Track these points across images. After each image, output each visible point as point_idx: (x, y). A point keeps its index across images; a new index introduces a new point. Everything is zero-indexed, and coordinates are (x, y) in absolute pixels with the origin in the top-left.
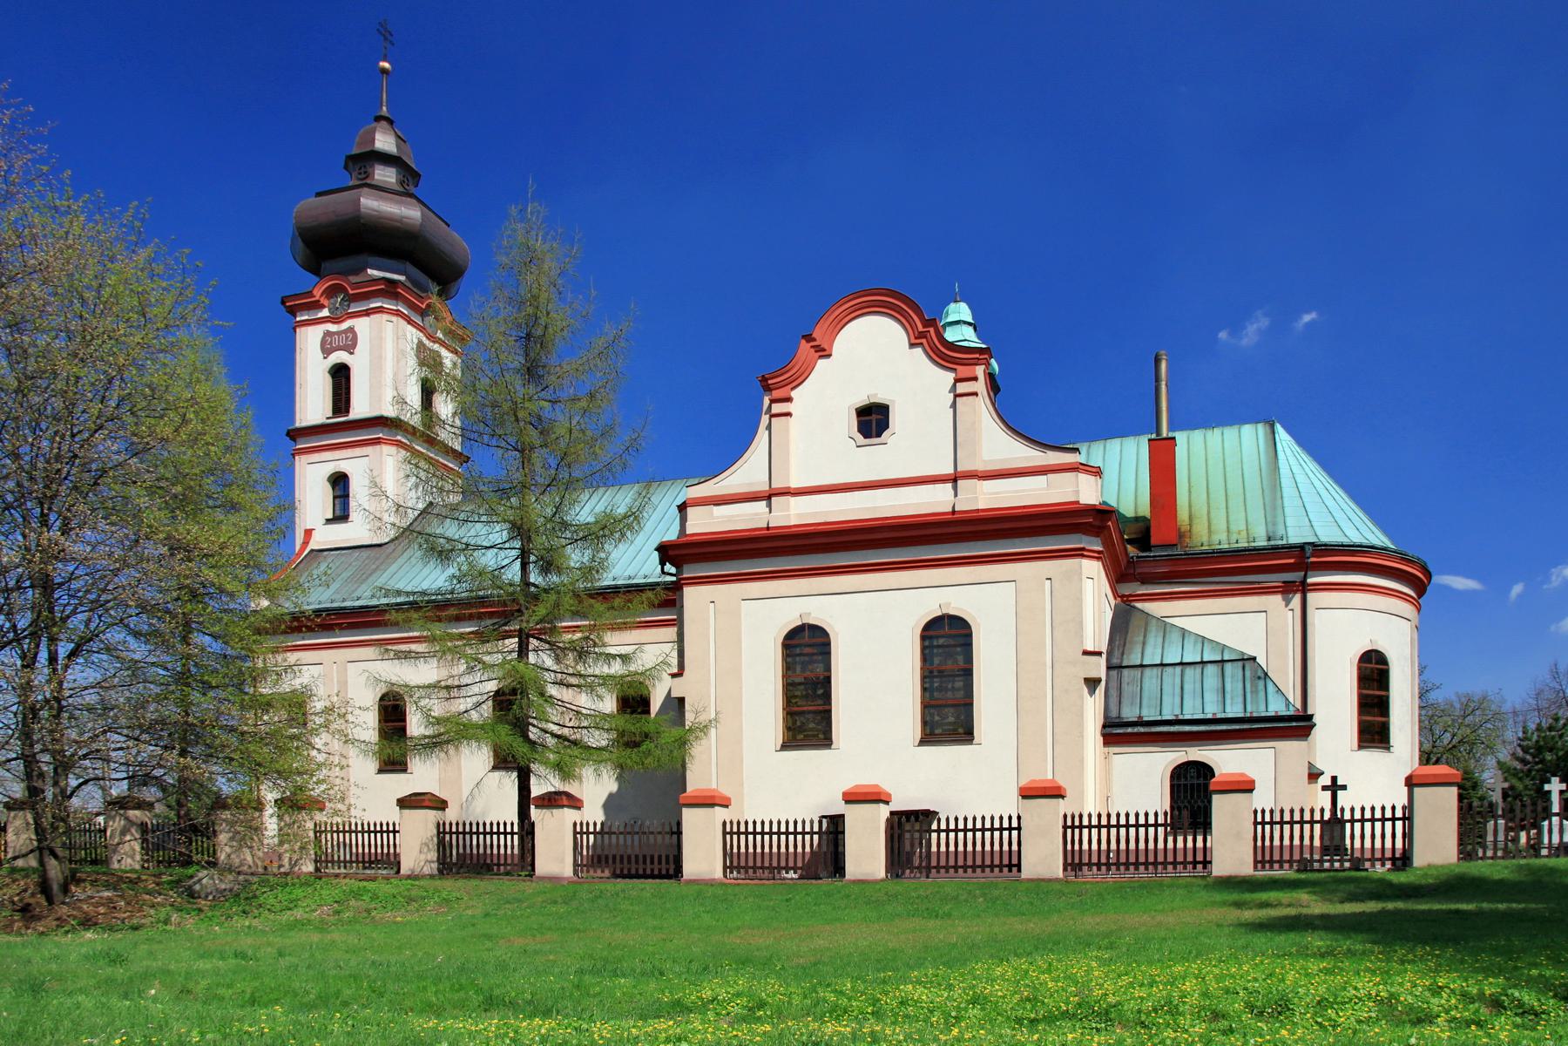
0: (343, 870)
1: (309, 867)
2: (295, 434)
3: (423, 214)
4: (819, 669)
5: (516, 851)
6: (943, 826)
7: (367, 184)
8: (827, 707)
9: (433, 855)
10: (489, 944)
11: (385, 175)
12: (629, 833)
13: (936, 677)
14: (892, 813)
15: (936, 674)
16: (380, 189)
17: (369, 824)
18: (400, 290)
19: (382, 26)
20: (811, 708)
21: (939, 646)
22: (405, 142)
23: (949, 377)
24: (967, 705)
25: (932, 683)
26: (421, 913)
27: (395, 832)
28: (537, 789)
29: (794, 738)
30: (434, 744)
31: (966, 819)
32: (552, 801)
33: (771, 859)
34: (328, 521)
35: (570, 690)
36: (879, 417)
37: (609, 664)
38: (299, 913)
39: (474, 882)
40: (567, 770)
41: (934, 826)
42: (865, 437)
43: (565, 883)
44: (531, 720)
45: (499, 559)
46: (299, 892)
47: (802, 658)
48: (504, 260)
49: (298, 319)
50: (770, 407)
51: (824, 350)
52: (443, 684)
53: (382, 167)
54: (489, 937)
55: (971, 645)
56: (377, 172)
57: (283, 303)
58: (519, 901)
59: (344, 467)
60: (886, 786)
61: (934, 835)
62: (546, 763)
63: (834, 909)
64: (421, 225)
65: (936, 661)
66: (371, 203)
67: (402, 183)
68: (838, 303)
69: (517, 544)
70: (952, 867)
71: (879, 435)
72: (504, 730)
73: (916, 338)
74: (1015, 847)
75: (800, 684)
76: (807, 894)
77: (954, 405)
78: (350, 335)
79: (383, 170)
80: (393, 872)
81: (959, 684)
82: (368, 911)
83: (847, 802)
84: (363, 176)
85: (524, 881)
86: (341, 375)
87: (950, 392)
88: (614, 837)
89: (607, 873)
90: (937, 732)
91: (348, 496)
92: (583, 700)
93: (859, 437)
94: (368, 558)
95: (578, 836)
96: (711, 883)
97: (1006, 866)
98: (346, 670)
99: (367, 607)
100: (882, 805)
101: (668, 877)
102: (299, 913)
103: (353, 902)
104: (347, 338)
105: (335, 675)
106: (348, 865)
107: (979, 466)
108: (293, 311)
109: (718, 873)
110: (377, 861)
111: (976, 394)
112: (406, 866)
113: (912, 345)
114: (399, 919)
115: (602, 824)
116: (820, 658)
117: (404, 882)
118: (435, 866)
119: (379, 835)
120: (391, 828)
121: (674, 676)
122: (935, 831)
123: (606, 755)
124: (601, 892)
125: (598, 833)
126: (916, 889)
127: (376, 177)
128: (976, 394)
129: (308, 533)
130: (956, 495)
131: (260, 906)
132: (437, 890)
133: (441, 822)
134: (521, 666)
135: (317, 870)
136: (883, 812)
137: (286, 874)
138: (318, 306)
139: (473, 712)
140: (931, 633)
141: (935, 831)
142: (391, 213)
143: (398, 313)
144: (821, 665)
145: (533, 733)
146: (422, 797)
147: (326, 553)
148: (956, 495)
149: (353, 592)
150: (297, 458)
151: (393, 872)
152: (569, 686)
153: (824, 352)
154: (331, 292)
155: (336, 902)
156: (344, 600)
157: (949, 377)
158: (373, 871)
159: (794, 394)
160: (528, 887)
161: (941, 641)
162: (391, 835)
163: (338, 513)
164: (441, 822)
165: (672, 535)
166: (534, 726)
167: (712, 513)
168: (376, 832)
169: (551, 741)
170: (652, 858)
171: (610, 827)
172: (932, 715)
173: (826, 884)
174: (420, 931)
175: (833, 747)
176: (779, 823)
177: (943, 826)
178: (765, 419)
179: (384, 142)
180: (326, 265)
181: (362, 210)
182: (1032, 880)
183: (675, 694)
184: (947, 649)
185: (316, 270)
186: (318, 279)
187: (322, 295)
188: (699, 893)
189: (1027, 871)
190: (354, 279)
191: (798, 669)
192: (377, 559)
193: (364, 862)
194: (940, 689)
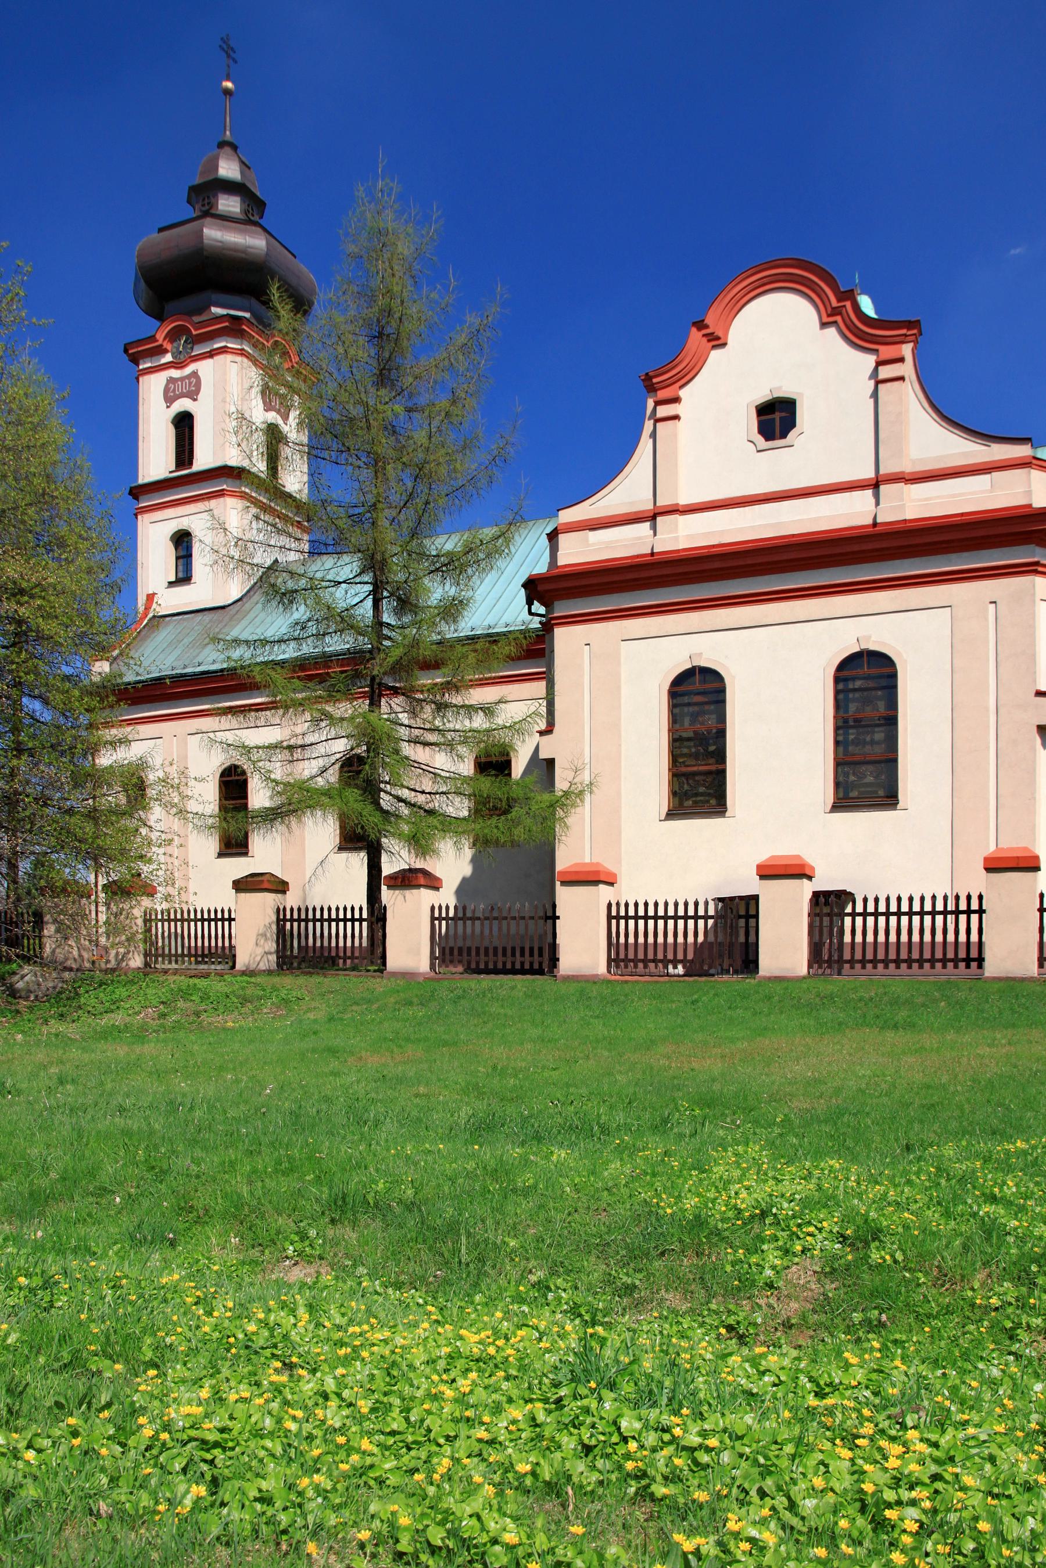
0: (174, 966)
1: (137, 961)
2: (138, 492)
3: (268, 244)
4: (711, 721)
5: (365, 944)
6: (859, 909)
7: (209, 213)
8: (720, 767)
9: (272, 946)
10: (334, 1064)
11: (229, 204)
12: (496, 918)
13: (852, 727)
14: (816, 895)
15: (851, 723)
16: (226, 219)
17: (202, 912)
18: (244, 327)
19: (224, 42)
20: (701, 768)
21: (855, 690)
22: (249, 168)
23: (869, 361)
24: (890, 761)
25: (846, 734)
26: (256, 1016)
27: (231, 920)
28: (389, 867)
29: (681, 805)
30: (273, 816)
31: (911, 899)
32: (406, 880)
33: (665, 951)
34: (171, 584)
35: (427, 748)
36: (783, 414)
37: (471, 719)
38: (118, 1018)
39: (316, 979)
40: (423, 842)
41: (849, 910)
42: (767, 440)
43: (421, 979)
44: (382, 786)
45: (349, 595)
46: (121, 992)
47: (691, 709)
48: (352, 248)
49: (141, 367)
50: (654, 410)
51: (718, 338)
52: (285, 744)
53: (226, 196)
54: (333, 1051)
55: (895, 687)
56: (220, 202)
57: (126, 351)
58: (369, 1001)
59: (184, 524)
60: (810, 857)
61: (848, 920)
62: (400, 836)
63: (755, 1014)
64: (267, 254)
65: (852, 708)
66: (214, 234)
67: (246, 212)
68: (734, 280)
69: (367, 577)
70: (870, 961)
71: (784, 435)
72: (353, 795)
73: (829, 316)
74: (974, 937)
75: (689, 739)
76: (716, 995)
77: (875, 395)
78: (194, 380)
79: (227, 200)
80: (227, 967)
81: (879, 735)
82: (197, 1014)
83: (763, 877)
84: (207, 207)
85: (373, 977)
86: (184, 424)
87: (870, 378)
88: (477, 923)
89: (460, 969)
90: (851, 795)
91: (191, 556)
92: (441, 760)
93: (760, 440)
94: (210, 621)
95: (437, 922)
96: (592, 980)
97: (963, 960)
98: (186, 744)
99: (208, 672)
100: (805, 881)
101: (540, 972)
102: (118, 1018)
103: (180, 1004)
104: (190, 383)
105: (175, 750)
106: (180, 959)
107: (908, 467)
108: (135, 360)
109: (602, 969)
110: (203, 956)
111: (902, 378)
112: (242, 960)
113: (824, 325)
114: (230, 1024)
115: (456, 907)
116: (712, 707)
117: (239, 978)
118: (273, 958)
119: (213, 923)
120: (226, 916)
121: (542, 733)
122: (848, 914)
123: (464, 826)
124: (464, 991)
125: (451, 919)
126: (855, 990)
127: (220, 207)
128: (902, 378)
129: (150, 597)
130: (877, 504)
131: (80, 1007)
132: (275, 989)
133: (281, 908)
134: (373, 717)
135: (147, 964)
136: (806, 889)
137: (113, 970)
138: (161, 351)
139: (319, 779)
140: (845, 673)
141: (848, 914)
142: (236, 243)
143: (242, 353)
144: (714, 716)
145: (386, 801)
146: (260, 878)
147: (168, 619)
148: (877, 504)
149: (195, 657)
150: (139, 517)
151: (227, 967)
152: (426, 744)
153: (717, 341)
154: (173, 336)
155: (163, 1003)
156: (185, 667)
157: (869, 361)
158: (205, 967)
159: (682, 393)
160: (378, 985)
161: (858, 684)
162: (226, 923)
163: (181, 575)
164: (281, 908)
165: (541, 568)
166: (386, 792)
167: (587, 540)
168: (209, 920)
169: (405, 811)
170: (504, 949)
171: (474, 911)
172: (847, 775)
173: (730, 983)
174: (251, 1042)
175: (727, 814)
176: (676, 905)
177: (859, 909)
178: (649, 425)
179: (228, 169)
180: (169, 307)
181: (205, 241)
182: (999, 979)
183: (543, 755)
184: (865, 693)
185: (160, 316)
186: (158, 323)
187: (165, 339)
188: (582, 992)
189: (991, 968)
190: (196, 319)
191: (687, 722)
192: (221, 622)
193: (196, 956)
194: (856, 742)
